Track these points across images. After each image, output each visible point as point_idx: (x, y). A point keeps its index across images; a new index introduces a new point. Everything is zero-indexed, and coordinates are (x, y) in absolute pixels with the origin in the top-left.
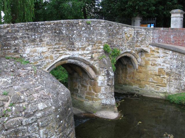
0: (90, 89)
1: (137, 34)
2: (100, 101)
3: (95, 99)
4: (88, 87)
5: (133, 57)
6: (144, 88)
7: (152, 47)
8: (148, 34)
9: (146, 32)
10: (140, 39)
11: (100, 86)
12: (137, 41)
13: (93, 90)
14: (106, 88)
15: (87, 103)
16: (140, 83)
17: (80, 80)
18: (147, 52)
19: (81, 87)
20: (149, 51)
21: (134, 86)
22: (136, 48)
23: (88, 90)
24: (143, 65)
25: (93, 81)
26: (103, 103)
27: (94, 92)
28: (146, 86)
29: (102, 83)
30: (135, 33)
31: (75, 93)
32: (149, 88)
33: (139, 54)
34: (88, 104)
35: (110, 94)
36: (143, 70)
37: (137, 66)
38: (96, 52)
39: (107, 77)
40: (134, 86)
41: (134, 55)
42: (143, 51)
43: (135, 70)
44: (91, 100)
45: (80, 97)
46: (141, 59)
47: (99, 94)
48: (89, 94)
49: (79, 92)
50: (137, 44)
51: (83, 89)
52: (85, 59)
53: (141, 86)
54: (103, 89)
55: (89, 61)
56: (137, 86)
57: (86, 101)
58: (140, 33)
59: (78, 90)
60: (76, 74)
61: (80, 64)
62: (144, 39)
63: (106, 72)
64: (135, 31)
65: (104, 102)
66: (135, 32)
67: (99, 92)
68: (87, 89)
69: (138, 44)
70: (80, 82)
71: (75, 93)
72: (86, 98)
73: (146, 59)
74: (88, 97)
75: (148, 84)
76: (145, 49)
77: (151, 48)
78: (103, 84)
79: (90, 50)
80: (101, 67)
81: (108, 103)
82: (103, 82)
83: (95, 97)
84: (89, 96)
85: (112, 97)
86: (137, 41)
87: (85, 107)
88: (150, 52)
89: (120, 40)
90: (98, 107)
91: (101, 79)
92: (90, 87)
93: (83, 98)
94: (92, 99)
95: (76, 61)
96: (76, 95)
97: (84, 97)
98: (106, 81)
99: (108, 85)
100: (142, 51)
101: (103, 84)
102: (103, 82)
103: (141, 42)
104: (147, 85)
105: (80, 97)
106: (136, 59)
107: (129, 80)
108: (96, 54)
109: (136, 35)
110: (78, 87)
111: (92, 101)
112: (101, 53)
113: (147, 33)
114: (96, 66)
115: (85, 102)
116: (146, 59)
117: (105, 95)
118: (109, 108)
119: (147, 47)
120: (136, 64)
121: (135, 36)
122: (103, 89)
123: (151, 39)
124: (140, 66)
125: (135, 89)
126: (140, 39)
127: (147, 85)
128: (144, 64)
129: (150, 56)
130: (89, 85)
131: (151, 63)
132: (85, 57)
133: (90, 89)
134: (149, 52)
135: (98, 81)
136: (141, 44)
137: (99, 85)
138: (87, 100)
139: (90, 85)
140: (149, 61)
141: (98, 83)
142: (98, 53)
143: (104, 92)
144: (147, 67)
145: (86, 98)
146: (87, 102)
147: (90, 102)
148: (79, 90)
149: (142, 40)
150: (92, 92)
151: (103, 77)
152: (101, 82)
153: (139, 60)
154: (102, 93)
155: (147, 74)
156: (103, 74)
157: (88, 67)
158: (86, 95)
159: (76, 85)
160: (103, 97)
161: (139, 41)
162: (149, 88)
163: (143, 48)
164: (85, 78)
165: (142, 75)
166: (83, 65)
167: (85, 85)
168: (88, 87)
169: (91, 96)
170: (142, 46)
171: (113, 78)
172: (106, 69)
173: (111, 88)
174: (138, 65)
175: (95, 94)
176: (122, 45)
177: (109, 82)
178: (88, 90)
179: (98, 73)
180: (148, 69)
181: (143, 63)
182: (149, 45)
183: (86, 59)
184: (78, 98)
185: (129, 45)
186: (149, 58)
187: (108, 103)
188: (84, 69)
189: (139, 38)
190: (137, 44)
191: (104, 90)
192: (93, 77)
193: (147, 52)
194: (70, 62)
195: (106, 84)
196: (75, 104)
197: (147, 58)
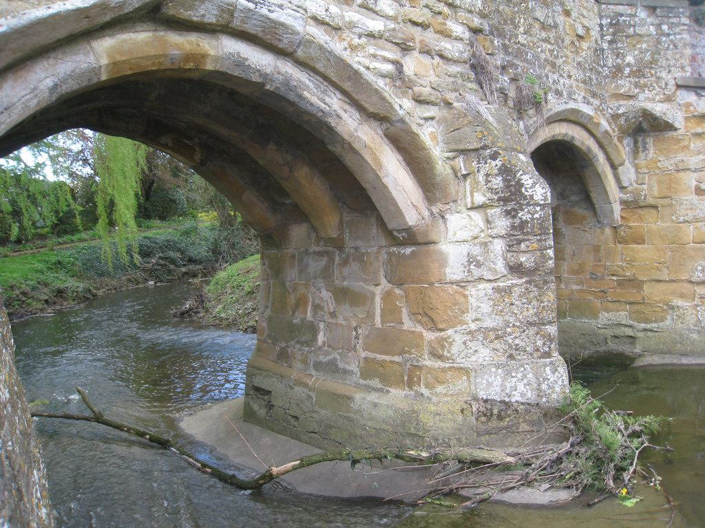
0: (391, 312)
1: (614, 34)
2: (461, 384)
3: (430, 369)
4: (378, 300)
5: (601, 157)
6: (663, 319)
7: (691, 97)
8: (668, 35)
9: (659, 26)
10: (629, 59)
11: (457, 283)
12: (618, 70)
13: (413, 314)
14: (508, 291)
15: (375, 405)
16: (639, 299)
17: (323, 262)
18: (669, 127)
19: (331, 306)
20: (679, 122)
21: (604, 317)
22: (614, 104)
23: (378, 319)
24: (650, 201)
25: (408, 250)
26: (482, 394)
27: (419, 328)
28: (672, 308)
29: (472, 260)
30: (601, 26)
31: (296, 350)
32: (691, 319)
33: (625, 142)
34: (381, 413)
35: (533, 330)
36: (651, 223)
37: (617, 208)
38: (427, 52)
39: (508, 213)
40: (604, 317)
41: (605, 142)
42: (645, 125)
43: (608, 231)
44: (399, 383)
45: (332, 368)
46: (637, 167)
47: (459, 339)
48: (387, 340)
49: (321, 338)
50: (617, 87)
51: (347, 315)
52: (357, 61)
53: (640, 308)
54: (479, 299)
55: (381, 83)
56: (623, 316)
57: (369, 389)
58: (630, 26)
59: (314, 331)
60: (298, 232)
61: (314, 100)
62: (648, 57)
63: (498, 182)
64: (601, 17)
65: (492, 386)
66: (604, 22)
67: (455, 322)
68: (370, 315)
69: (625, 85)
70: (326, 274)
71: (296, 350)
72: (369, 370)
73: (667, 164)
74: (382, 364)
75: (682, 296)
76: (658, 109)
77: (688, 105)
78: (479, 265)
79: (387, 17)
80: (462, 147)
81: (522, 395)
82: (477, 250)
83: (428, 362)
84: (387, 358)
85: (548, 355)
86: (618, 70)
87: (363, 427)
88: (686, 127)
89: (544, 35)
90: (450, 424)
91: (465, 235)
92: (387, 296)
93: (345, 372)
94: (410, 378)
95: (288, 69)
96: (305, 362)
97: (353, 367)
98: (499, 246)
99: (516, 269)
100: (647, 128)
101: (479, 265)
102: (477, 250)
103: (638, 73)
104: (680, 302)
105: (332, 368)
106: (614, 167)
107: (575, 287)
108: (426, 60)
109: (608, 38)
110: (317, 308)
111: (407, 391)
112: (455, 69)
113: (665, 27)
114: (430, 136)
115: (358, 396)
116: (667, 164)
117: (497, 338)
118: (527, 428)
119: (668, 99)
120: (611, 198)
121: (605, 46)
122: (479, 299)
123: (685, 62)
124: (632, 206)
125: (609, 333)
126: (629, 59)
127: (680, 302)
128: (656, 193)
129: (687, 147)
130: (385, 284)
131: (694, 183)
132: (353, 48)
133: (391, 312)
134: (677, 125)
135: (444, 247)
136: (636, 85)
137: (454, 270)
138: (376, 383)
139: (389, 282)
140: (682, 174)
141: (443, 261)
142: (437, 59)
143: (489, 323)
144: (671, 205)
145: (369, 370)
146: (373, 397)
147: (397, 397)
148: (322, 325)
149: (640, 61)
150: (408, 324)
151: (477, 217)
152: (464, 249)
153: (628, 173)
154: (473, 326)
155: (677, 244)
156: (480, 199)
157: (378, 139)
158: (363, 354)
159: (301, 302)
160: (484, 354)
161: (627, 71)
162: (691, 319)
163: (649, 106)
164: (359, 243)
165: (644, 252)
166: (345, 116)
167: (359, 286)
168: (378, 300)
169: (397, 359)
170: (641, 97)
171: (543, 220)
172: (494, 157)
173: (535, 291)
174: (623, 202)
175: (429, 336)
176: (553, 65)
177: (523, 246)
178: (378, 319)
179: (444, 189)
180: (683, 213)
181: (650, 190)
182: (679, 87)
183: (362, 70)
184: (317, 379)
185: (584, 82)
186: (680, 157)
187: (522, 395)
188: (349, 160)
189: (624, 56)
190: (617, 87)
191: (486, 307)
192: (411, 218)
193: (676, 129)
194: (241, 63)
195: (500, 266)
196: (296, 418)
197: (668, 159)
